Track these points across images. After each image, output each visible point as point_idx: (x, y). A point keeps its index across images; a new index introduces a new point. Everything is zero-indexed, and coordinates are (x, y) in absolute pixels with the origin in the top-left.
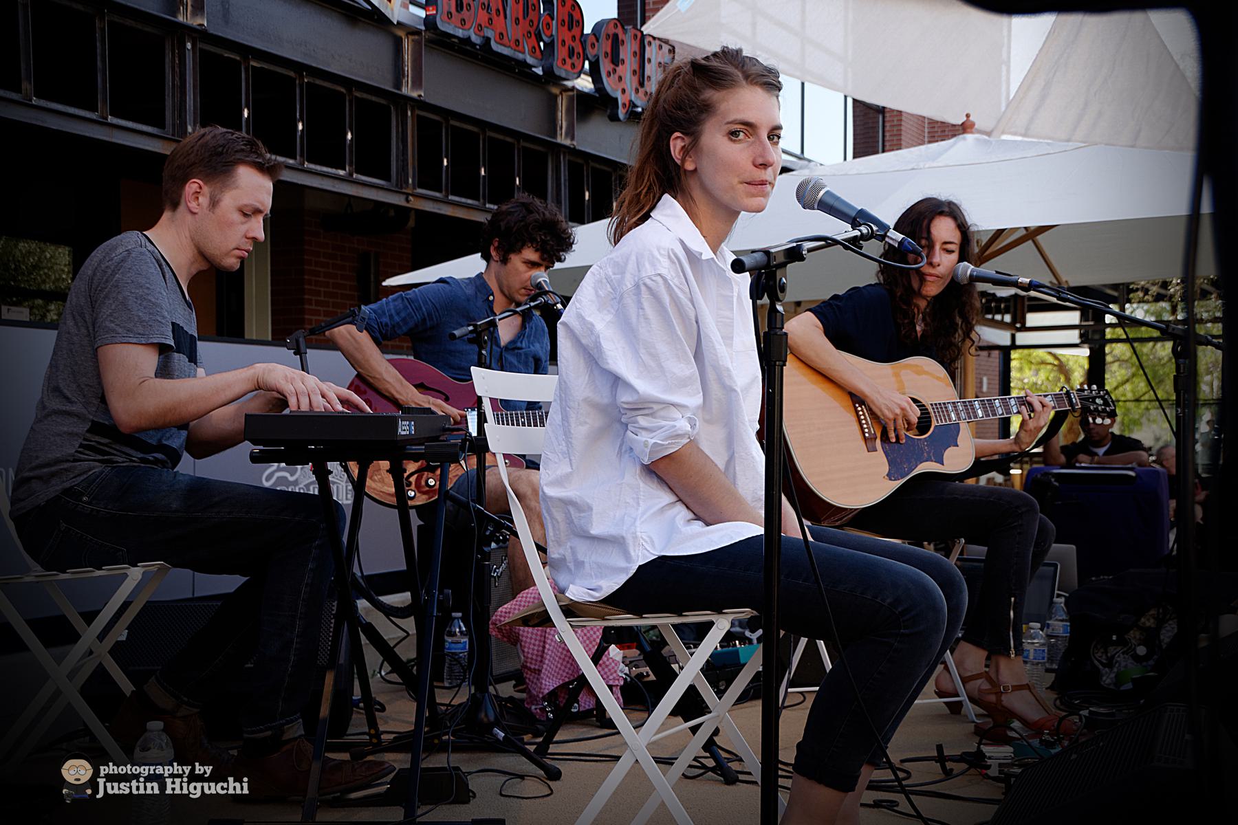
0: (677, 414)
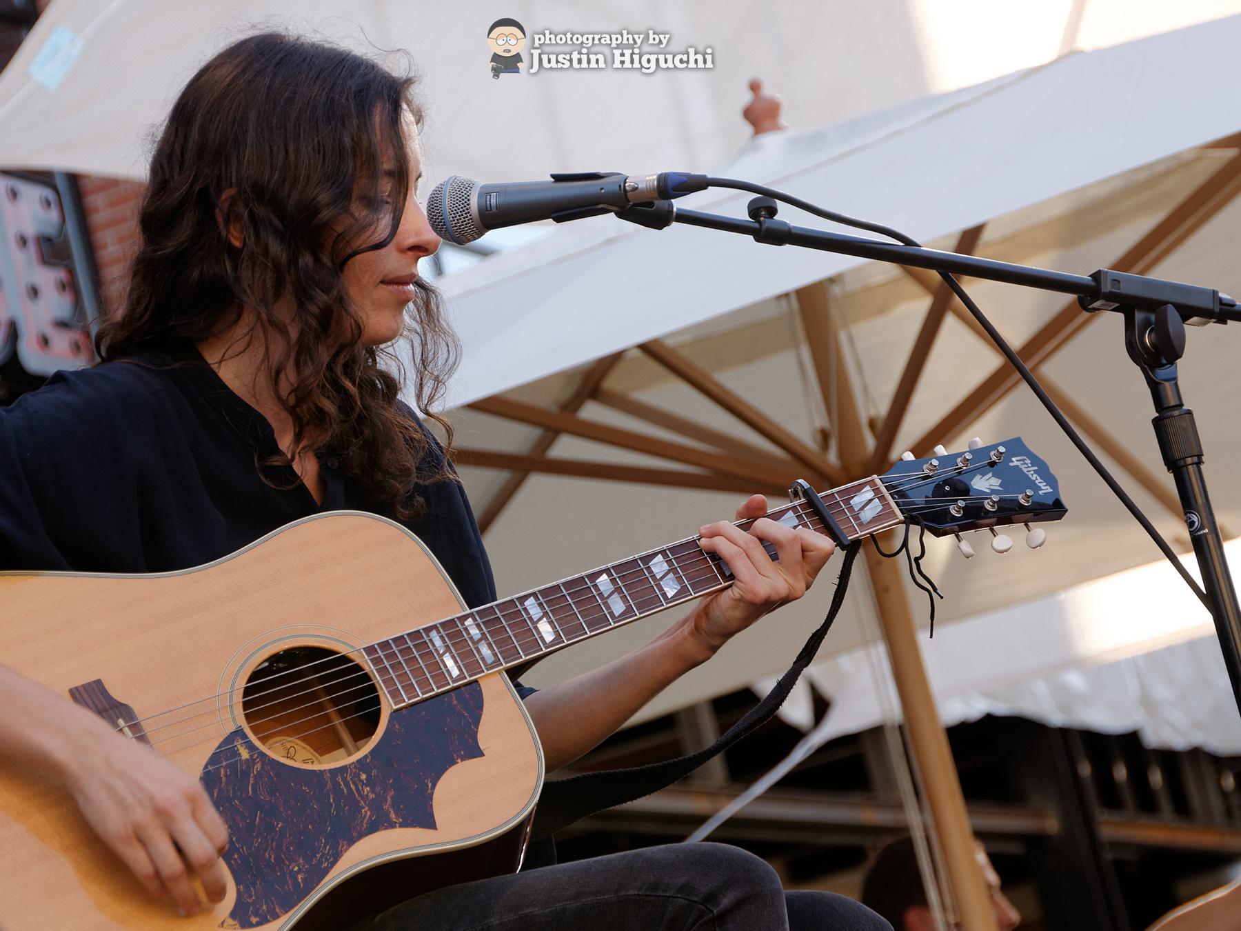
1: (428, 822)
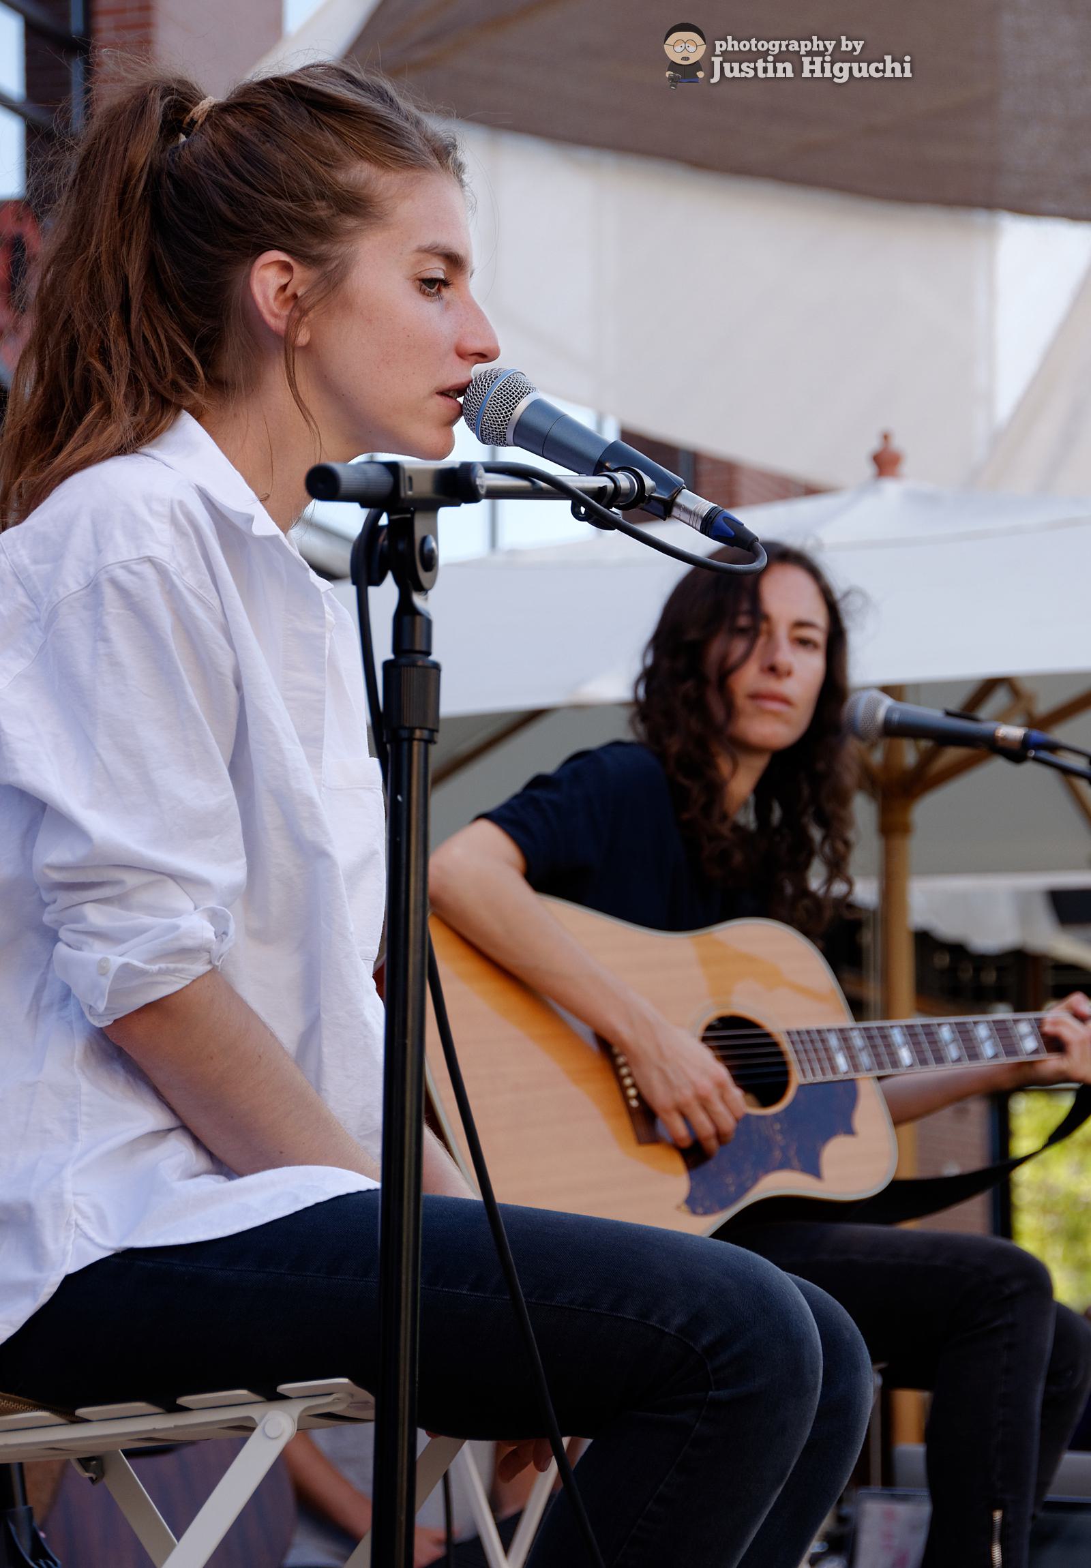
0: (178, 899)
1: (813, 1168)
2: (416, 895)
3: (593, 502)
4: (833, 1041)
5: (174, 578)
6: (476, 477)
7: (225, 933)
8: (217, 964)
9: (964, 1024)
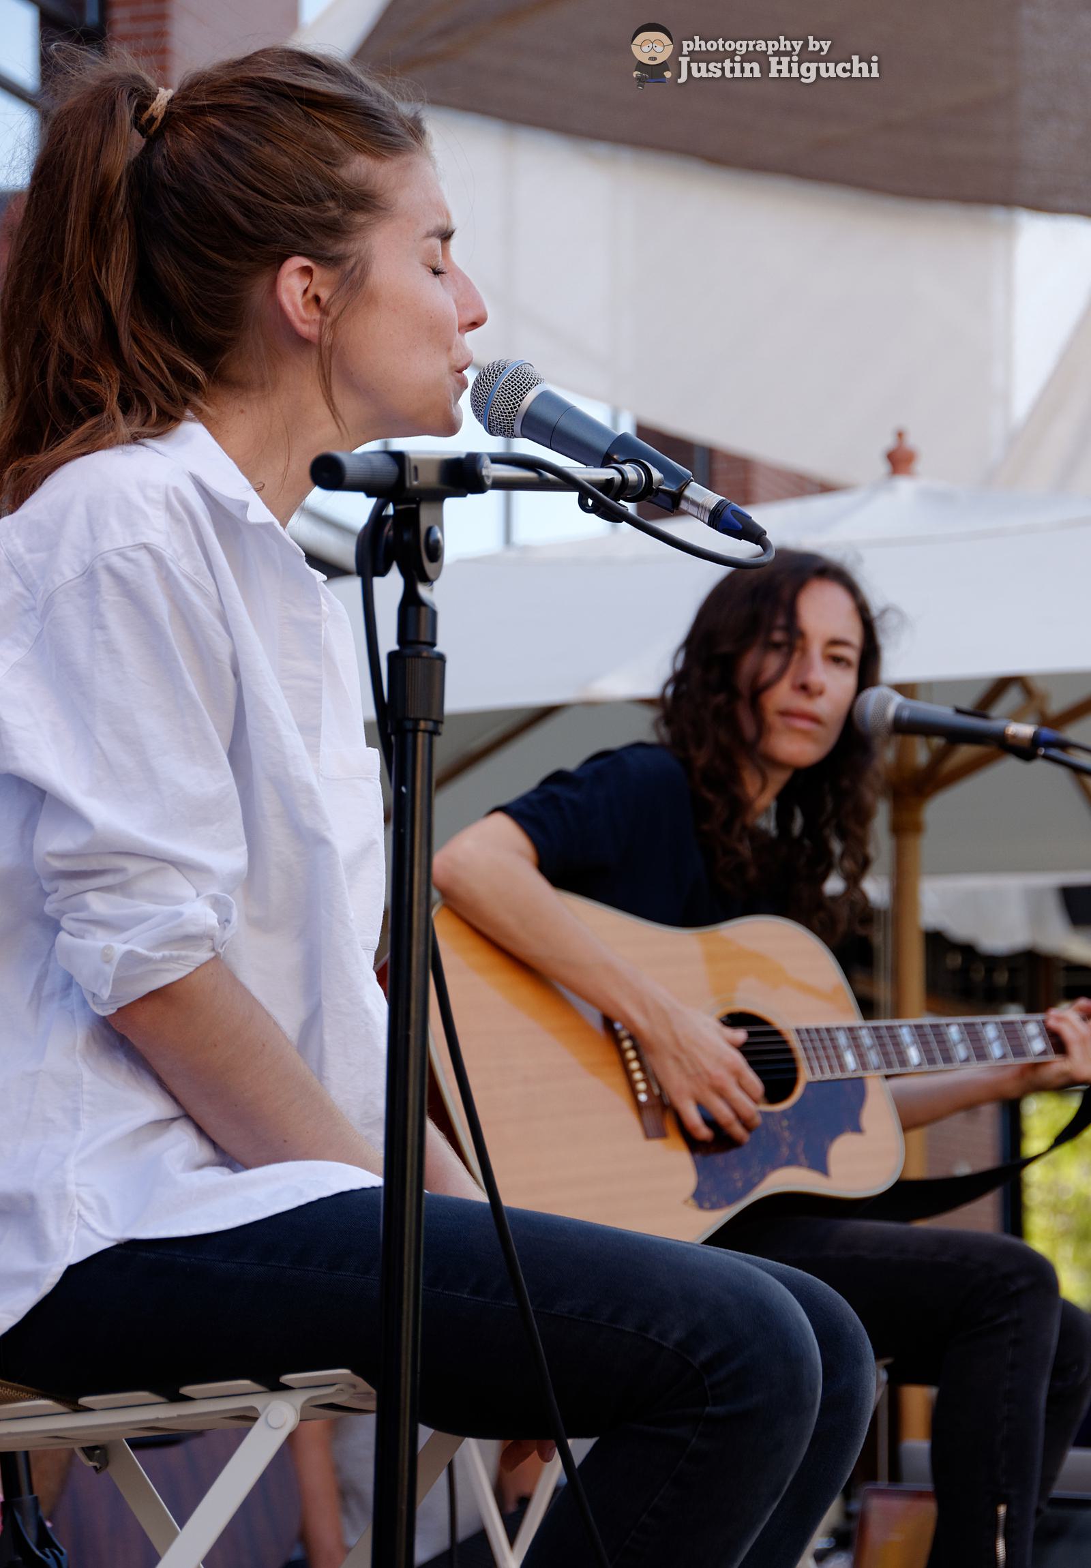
0: (180, 885)
1: (820, 1165)
2: (420, 887)
3: (601, 494)
4: (842, 1039)
5: (171, 564)
6: (482, 467)
7: (228, 921)
8: (221, 951)
9: (973, 1025)
